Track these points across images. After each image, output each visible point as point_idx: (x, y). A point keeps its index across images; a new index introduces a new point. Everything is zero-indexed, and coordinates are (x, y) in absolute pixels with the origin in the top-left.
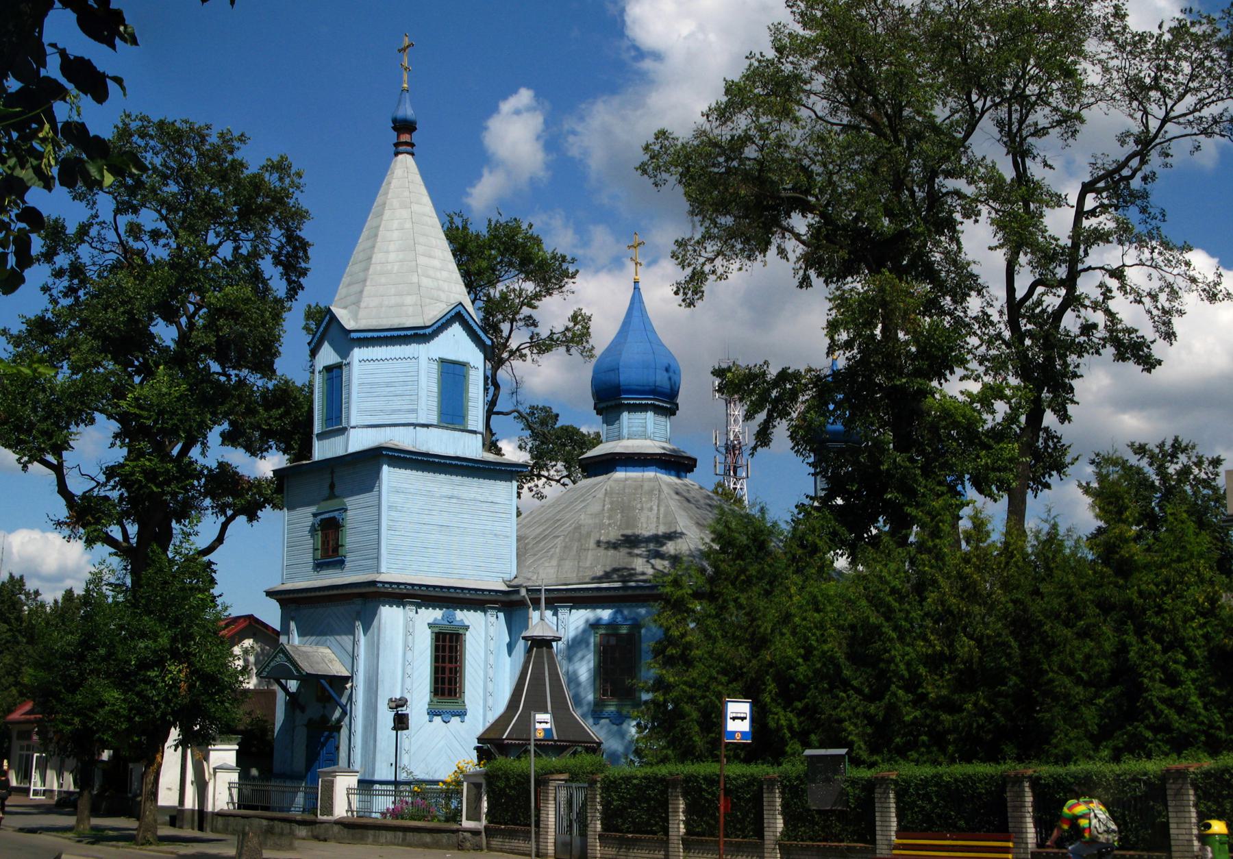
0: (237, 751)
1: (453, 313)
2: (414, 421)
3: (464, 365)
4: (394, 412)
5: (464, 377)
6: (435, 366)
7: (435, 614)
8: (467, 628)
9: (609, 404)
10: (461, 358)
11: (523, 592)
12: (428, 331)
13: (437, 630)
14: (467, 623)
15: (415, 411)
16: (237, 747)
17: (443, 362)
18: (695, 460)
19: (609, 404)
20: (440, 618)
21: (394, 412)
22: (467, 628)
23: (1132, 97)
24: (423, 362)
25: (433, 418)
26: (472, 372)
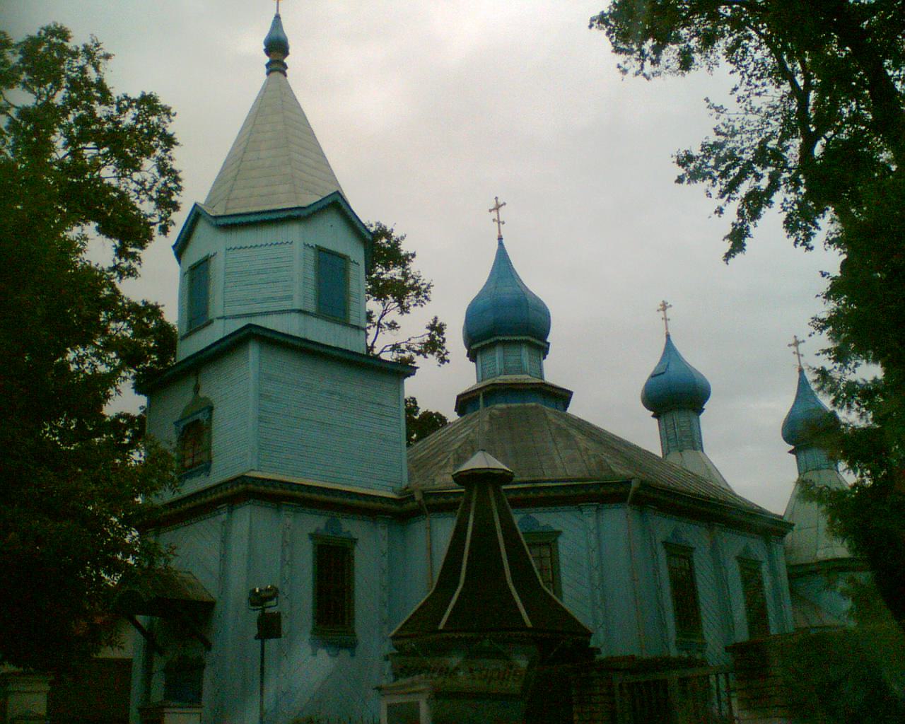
0: (49, 694)
1: (330, 200)
2: (290, 308)
3: (344, 258)
4: (265, 300)
5: (345, 271)
6: (311, 254)
7: (316, 522)
8: (354, 541)
9: (483, 343)
10: (341, 249)
11: (418, 497)
12: (305, 213)
13: (319, 542)
14: (355, 536)
15: (290, 298)
16: (48, 688)
17: (320, 251)
18: (571, 393)
19: (483, 343)
20: (322, 527)
21: (265, 300)
22: (354, 541)
23: (470, 672)
24: (298, 248)
25: (311, 307)
26: (353, 267)
